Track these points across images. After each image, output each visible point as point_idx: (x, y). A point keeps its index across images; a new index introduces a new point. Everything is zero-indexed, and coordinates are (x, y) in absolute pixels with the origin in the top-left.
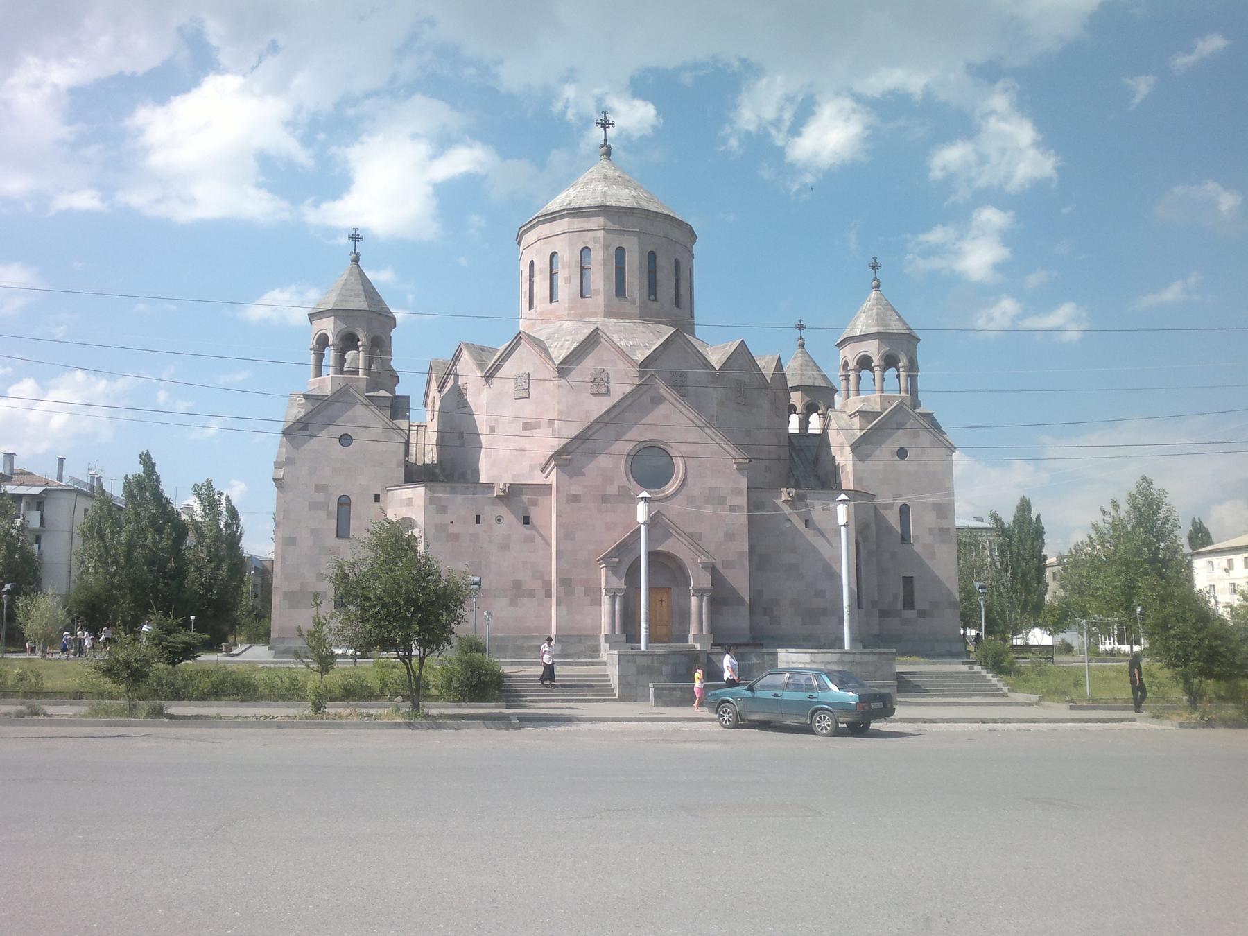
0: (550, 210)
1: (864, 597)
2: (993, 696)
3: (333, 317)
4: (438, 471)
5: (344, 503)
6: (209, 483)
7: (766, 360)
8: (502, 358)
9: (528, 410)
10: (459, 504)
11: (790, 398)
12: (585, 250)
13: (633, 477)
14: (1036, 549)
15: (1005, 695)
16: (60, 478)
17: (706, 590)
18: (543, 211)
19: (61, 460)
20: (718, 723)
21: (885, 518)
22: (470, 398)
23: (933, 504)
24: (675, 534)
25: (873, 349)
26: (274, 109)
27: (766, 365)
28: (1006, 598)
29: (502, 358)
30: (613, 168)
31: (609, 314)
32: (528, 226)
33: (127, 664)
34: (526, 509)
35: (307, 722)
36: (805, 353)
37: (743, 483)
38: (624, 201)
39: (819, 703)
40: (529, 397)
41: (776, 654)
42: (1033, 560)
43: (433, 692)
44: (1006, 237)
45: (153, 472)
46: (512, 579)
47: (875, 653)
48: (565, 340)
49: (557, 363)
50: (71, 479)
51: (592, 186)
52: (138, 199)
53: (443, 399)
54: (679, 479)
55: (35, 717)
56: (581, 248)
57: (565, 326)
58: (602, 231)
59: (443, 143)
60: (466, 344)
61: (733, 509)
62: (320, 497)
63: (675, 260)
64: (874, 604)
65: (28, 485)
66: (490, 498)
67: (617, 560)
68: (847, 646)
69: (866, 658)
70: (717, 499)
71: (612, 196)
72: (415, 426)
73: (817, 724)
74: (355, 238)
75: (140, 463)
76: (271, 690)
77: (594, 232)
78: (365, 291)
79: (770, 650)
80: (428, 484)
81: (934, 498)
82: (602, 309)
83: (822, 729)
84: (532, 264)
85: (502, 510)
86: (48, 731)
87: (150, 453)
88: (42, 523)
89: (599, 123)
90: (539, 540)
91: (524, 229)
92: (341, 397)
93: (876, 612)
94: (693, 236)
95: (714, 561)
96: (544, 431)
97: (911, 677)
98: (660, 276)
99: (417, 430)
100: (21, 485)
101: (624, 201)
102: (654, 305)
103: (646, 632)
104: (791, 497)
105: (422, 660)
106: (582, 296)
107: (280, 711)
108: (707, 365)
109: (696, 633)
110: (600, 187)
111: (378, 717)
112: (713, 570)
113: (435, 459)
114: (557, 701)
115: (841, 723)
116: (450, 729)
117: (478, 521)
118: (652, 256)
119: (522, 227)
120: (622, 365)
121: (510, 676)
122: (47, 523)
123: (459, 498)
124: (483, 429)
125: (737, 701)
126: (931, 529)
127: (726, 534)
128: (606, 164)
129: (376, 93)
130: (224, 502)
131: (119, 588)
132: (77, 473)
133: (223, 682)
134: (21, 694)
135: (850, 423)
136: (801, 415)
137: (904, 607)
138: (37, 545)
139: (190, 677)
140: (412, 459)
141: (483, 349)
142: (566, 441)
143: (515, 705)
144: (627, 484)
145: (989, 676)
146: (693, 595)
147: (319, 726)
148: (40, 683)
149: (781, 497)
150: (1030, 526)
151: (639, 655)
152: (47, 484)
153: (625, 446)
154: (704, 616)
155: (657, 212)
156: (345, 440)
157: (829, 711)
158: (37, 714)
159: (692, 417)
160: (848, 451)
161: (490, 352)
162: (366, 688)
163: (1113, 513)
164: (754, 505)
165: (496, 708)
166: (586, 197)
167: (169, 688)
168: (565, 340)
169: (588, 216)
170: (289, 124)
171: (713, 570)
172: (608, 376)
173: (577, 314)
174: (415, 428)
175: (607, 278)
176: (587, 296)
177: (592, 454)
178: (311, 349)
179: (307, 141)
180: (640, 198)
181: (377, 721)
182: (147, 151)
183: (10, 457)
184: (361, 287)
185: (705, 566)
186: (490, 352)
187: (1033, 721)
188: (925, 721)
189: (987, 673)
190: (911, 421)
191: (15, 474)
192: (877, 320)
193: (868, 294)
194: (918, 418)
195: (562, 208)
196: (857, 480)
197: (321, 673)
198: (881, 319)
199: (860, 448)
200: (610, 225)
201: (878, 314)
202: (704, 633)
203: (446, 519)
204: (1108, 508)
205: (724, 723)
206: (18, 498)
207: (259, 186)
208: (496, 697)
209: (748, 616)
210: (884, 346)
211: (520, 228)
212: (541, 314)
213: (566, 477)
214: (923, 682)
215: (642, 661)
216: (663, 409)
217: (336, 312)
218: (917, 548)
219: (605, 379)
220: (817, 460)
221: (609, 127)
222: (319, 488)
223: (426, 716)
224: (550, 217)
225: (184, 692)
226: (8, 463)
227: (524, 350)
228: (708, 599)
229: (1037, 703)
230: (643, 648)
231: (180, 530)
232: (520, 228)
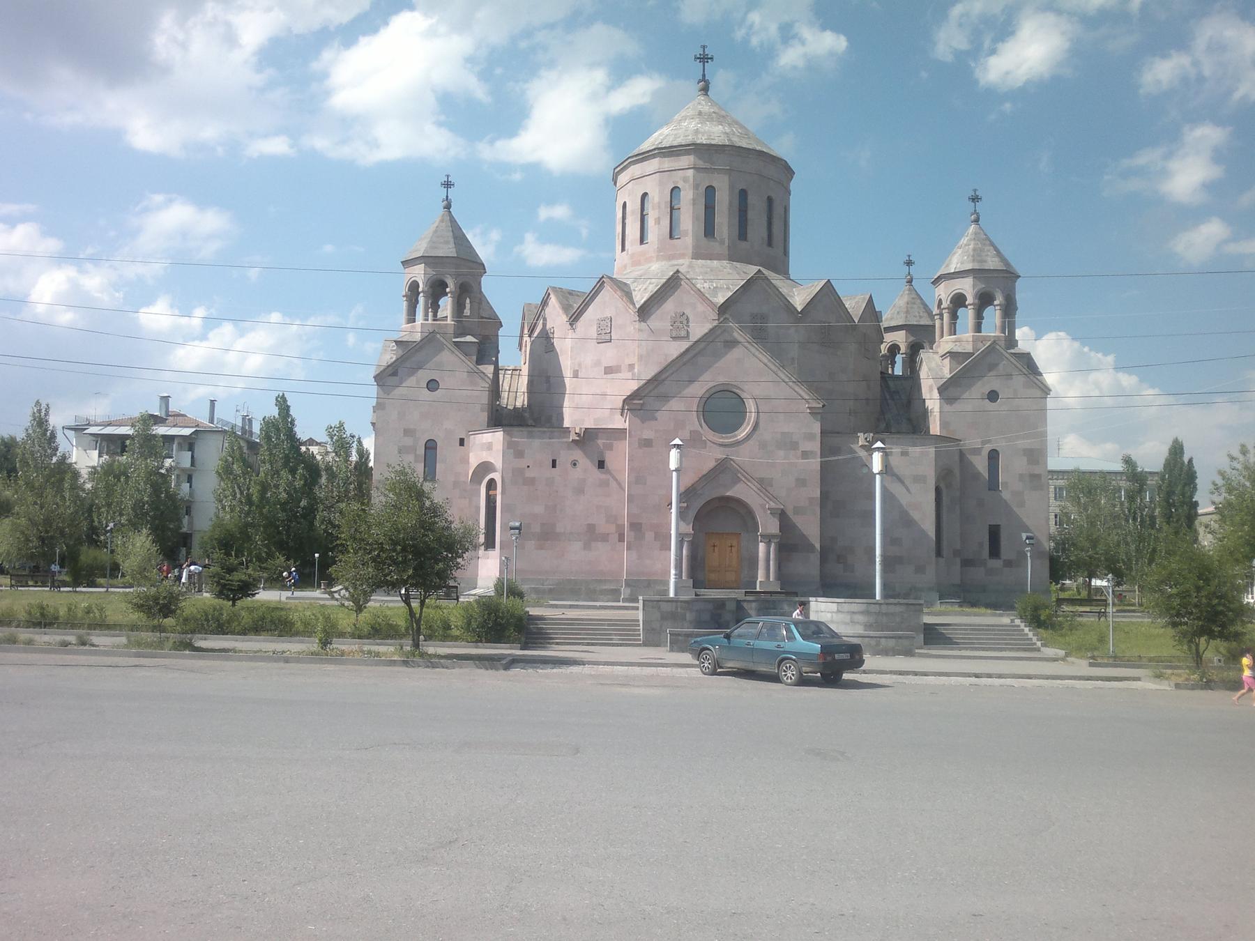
0: (642, 149)
1: (945, 543)
2: (1025, 650)
3: (423, 265)
4: (527, 415)
5: (431, 446)
6: (341, 425)
7: (856, 300)
8: (585, 302)
9: (609, 354)
10: (536, 447)
11: (883, 338)
12: (675, 190)
13: (705, 421)
14: (1187, 495)
15: (1038, 650)
16: (212, 421)
17: (774, 536)
18: (636, 152)
19: (213, 402)
20: (699, 669)
21: (971, 463)
22: (557, 343)
23: (1024, 450)
24: (743, 479)
25: (967, 287)
26: (460, 44)
27: (854, 305)
28: (1133, 547)
29: (585, 302)
30: (710, 104)
31: (697, 255)
32: (622, 166)
33: (156, 599)
34: (602, 454)
35: (314, 657)
36: (912, 290)
37: (816, 428)
38: (716, 138)
39: (785, 652)
40: (610, 342)
41: (809, 602)
42: (1183, 506)
43: (455, 632)
44: (1218, 156)
45: (288, 415)
46: (586, 523)
47: (901, 604)
48: (650, 283)
49: (638, 306)
50: (220, 420)
51: (686, 124)
52: (320, 142)
53: (532, 343)
54: (751, 424)
55: (82, 647)
56: (707, 185)
57: (653, 268)
58: (692, 170)
59: (621, 72)
60: (554, 289)
61: (805, 455)
62: (408, 441)
63: (768, 197)
64: (956, 553)
65: (180, 427)
66: (566, 442)
67: (685, 505)
68: (878, 597)
69: (892, 609)
70: (788, 443)
71: (703, 134)
72: (510, 370)
73: (783, 673)
74: (448, 185)
75: (276, 405)
76: (306, 627)
77: (684, 171)
78: (455, 238)
79: (803, 599)
80: (507, 429)
81: (1023, 443)
82: (690, 251)
83: (787, 679)
84: (625, 205)
85: (577, 454)
86: (93, 659)
87: (286, 396)
88: (193, 464)
89: (698, 58)
90: (613, 484)
91: (619, 169)
92: (431, 339)
93: (958, 560)
94: (788, 172)
95: (782, 507)
96: (626, 374)
97: (945, 629)
98: (751, 214)
99: (512, 375)
100: (174, 426)
101: (716, 138)
102: (744, 245)
103: (676, 578)
104: (868, 442)
105: (422, 603)
106: (671, 237)
107: (293, 646)
108: (789, 307)
109: (763, 580)
110: (693, 125)
111: (378, 654)
112: (782, 516)
113: (526, 403)
114: (583, 644)
115: (805, 673)
116: (443, 668)
117: (554, 465)
118: (743, 194)
119: (617, 167)
120: (701, 307)
121: (545, 619)
122: (197, 462)
123: (537, 442)
124: (567, 373)
125: (715, 648)
126: (1021, 476)
127: (797, 480)
128: (703, 100)
129: (551, 26)
130: (355, 445)
131: (252, 525)
132: (229, 416)
133: (263, 619)
134: (86, 626)
135: (941, 364)
136: (904, 356)
137: (990, 556)
138: (188, 484)
139: (233, 613)
140: (504, 402)
141: (571, 293)
142: (643, 382)
143: (533, 647)
144: (700, 429)
145: (1026, 630)
146: (761, 542)
147: (321, 661)
148: (104, 616)
149: (858, 441)
150: (1182, 471)
151: (663, 601)
152: (197, 426)
153: (699, 389)
154: (771, 563)
155: (749, 149)
156: (432, 385)
157: (794, 660)
158: (84, 644)
159: (766, 361)
160: (936, 394)
161: (578, 296)
162: (391, 626)
163: (1241, 458)
164: (827, 450)
165: (511, 649)
166: (678, 136)
167: (214, 623)
168: (650, 283)
169: (678, 155)
170: (470, 60)
171: (782, 516)
172: (688, 319)
173: (664, 254)
174: (510, 372)
175: (695, 218)
176: (676, 237)
177: (666, 398)
178: (404, 296)
179: (485, 75)
180: (734, 134)
181: (376, 658)
182: (328, 93)
183: (165, 399)
184: (451, 234)
185: (773, 512)
186: (578, 296)
187: (1029, 677)
188: (916, 674)
189: (1025, 626)
190: (1004, 362)
191: (170, 416)
192: (973, 256)
193: (967, 228)
194: (1012, 359)
195: (653, 148)
196: (944, 424)
197: (356, 612)
198: (977, 255)
199: (948, 390)
200: (701, 164)
201: (974, 250)
202: (771, 580)
203: (522, 463)
204: (1236, 453)
205: (704, 670)
206: (171, 439)
207: (440, 124)
208: (511, 639)
209: (818, 563)
210: (979, 283)
211: (615, 169)
212: (632, 256)
213: (638, 421)
214: (957, 634)
215: (666, 607)
216: (736, 353)
217: (426, 260)
218: (1006, 495)
219: (685, 322)
220: (909, 402)
221: (707, 62)
222: (408, 432)
223: (422, 655)
224: (641, 157)
225: (227, 627)
226: (164, 406)
227: (607, 293)
228: (688, 546)
229: (1063, 659)
230: (672, 595)
231: (313, 470)
232: (615, 169)
